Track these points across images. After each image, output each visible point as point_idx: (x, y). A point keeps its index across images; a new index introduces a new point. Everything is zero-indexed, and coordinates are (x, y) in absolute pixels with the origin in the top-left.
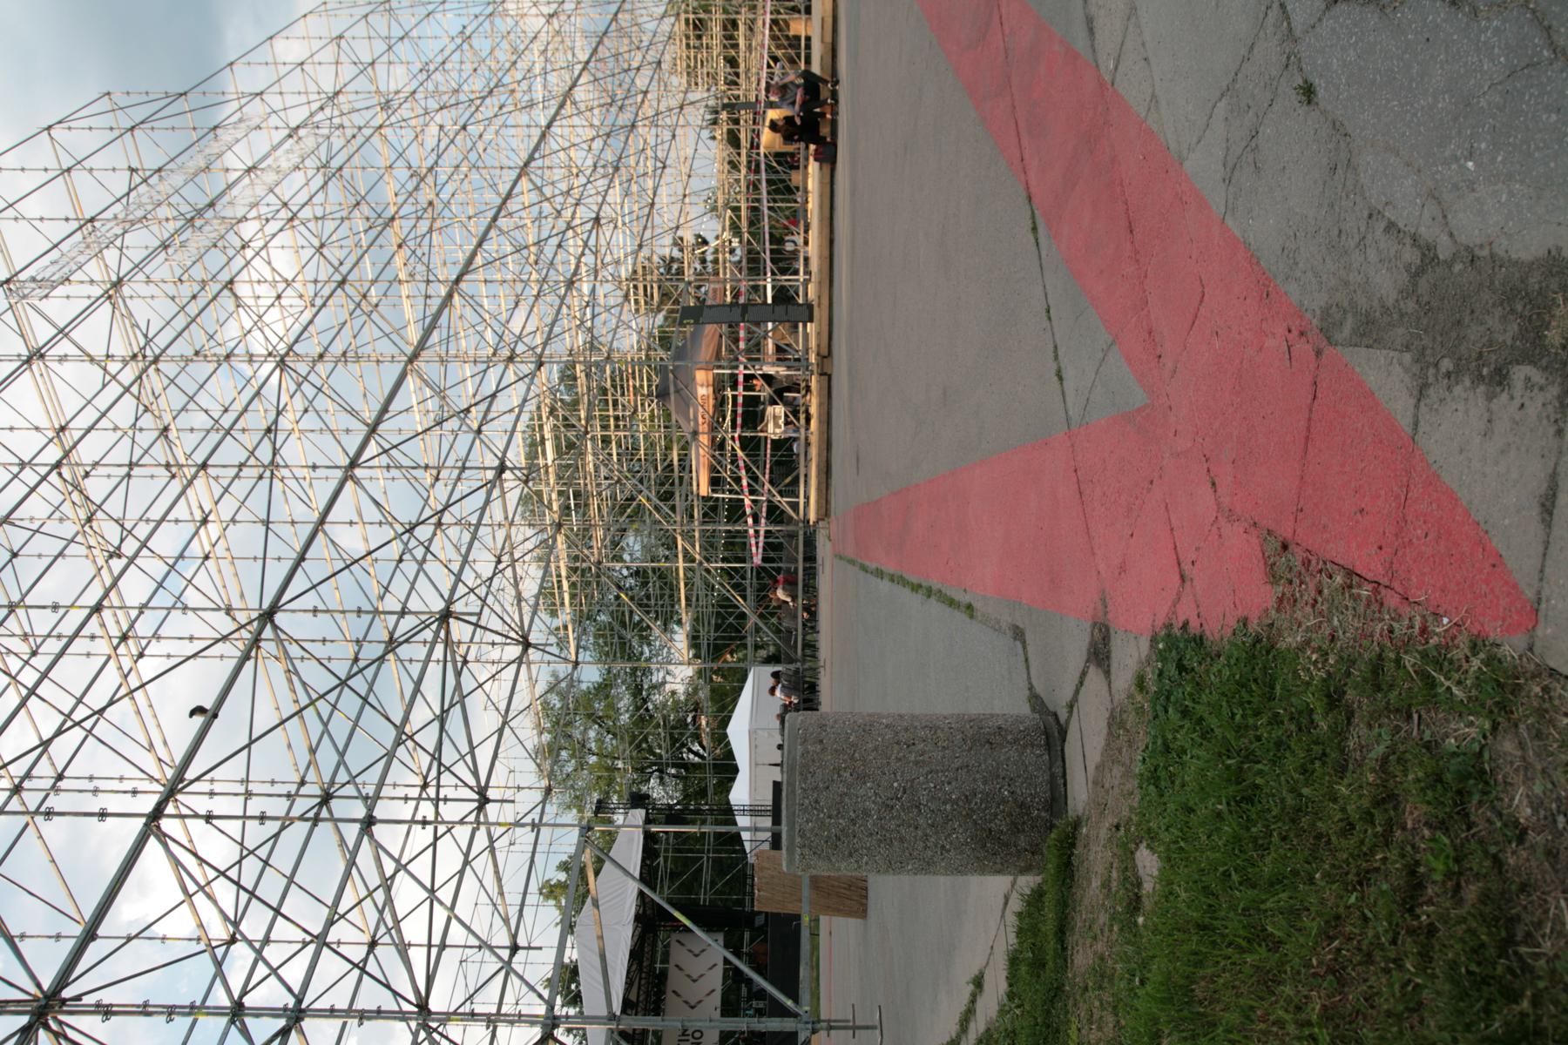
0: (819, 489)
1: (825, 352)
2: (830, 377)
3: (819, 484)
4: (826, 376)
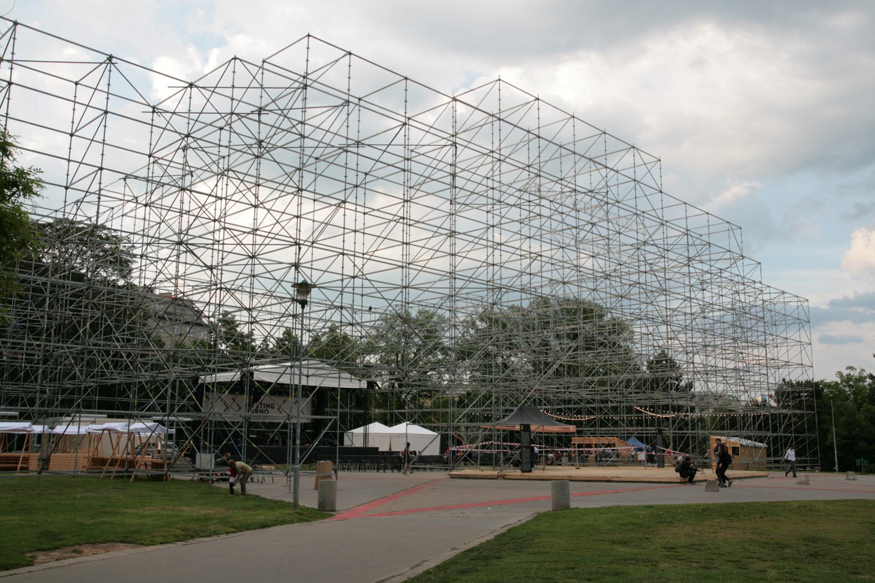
4: (497, 478)
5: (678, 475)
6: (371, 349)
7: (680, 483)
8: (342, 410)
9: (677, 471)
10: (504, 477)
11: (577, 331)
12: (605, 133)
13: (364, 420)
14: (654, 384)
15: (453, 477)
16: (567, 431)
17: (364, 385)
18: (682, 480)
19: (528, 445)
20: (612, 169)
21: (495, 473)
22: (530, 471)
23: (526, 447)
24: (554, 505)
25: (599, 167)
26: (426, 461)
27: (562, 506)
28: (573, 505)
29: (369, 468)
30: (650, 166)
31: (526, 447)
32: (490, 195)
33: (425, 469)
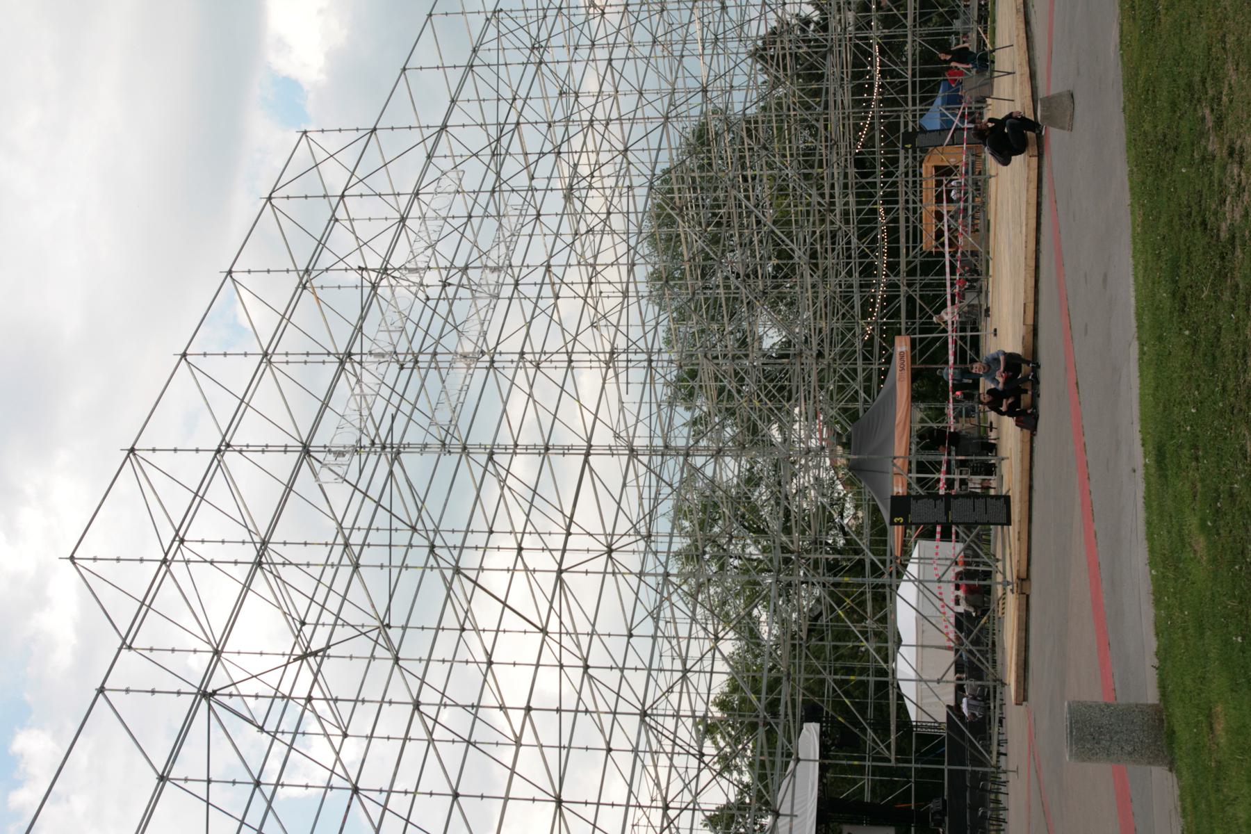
0: (1017, 682)
1: (1023, 575)
2: (1028, 597)
3: (1018, 677)
5: (1017, 160)
6: (750, 633)
7: (1040, 156)
8: (872, 687)
9: (1006, 162)
10: (1024, 579)
11: (712, 228)
12: (230, 272)
13: (886, 684)
14: (812, 75)
15: (1023, 697)
16: (907, 359)
17: (810, 738)
18: (1032, 149)
19: (941, 505)
20: (321, 244)
21: (1012, 602)
22: (1007, 499)
23: (948, 508)
24: (1154, 760)
25: (430, 143)
26: (976, 585)
27: (1155, 735)
28: (1151, 696)
29: (999, 806)
30: (320, 156)
31: (948, 508)
32: (373, 537)
33: (1001, 722)
